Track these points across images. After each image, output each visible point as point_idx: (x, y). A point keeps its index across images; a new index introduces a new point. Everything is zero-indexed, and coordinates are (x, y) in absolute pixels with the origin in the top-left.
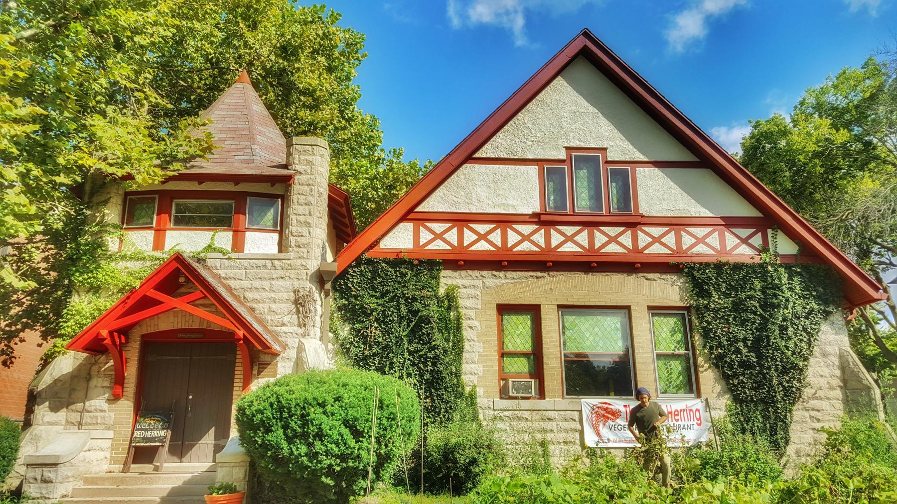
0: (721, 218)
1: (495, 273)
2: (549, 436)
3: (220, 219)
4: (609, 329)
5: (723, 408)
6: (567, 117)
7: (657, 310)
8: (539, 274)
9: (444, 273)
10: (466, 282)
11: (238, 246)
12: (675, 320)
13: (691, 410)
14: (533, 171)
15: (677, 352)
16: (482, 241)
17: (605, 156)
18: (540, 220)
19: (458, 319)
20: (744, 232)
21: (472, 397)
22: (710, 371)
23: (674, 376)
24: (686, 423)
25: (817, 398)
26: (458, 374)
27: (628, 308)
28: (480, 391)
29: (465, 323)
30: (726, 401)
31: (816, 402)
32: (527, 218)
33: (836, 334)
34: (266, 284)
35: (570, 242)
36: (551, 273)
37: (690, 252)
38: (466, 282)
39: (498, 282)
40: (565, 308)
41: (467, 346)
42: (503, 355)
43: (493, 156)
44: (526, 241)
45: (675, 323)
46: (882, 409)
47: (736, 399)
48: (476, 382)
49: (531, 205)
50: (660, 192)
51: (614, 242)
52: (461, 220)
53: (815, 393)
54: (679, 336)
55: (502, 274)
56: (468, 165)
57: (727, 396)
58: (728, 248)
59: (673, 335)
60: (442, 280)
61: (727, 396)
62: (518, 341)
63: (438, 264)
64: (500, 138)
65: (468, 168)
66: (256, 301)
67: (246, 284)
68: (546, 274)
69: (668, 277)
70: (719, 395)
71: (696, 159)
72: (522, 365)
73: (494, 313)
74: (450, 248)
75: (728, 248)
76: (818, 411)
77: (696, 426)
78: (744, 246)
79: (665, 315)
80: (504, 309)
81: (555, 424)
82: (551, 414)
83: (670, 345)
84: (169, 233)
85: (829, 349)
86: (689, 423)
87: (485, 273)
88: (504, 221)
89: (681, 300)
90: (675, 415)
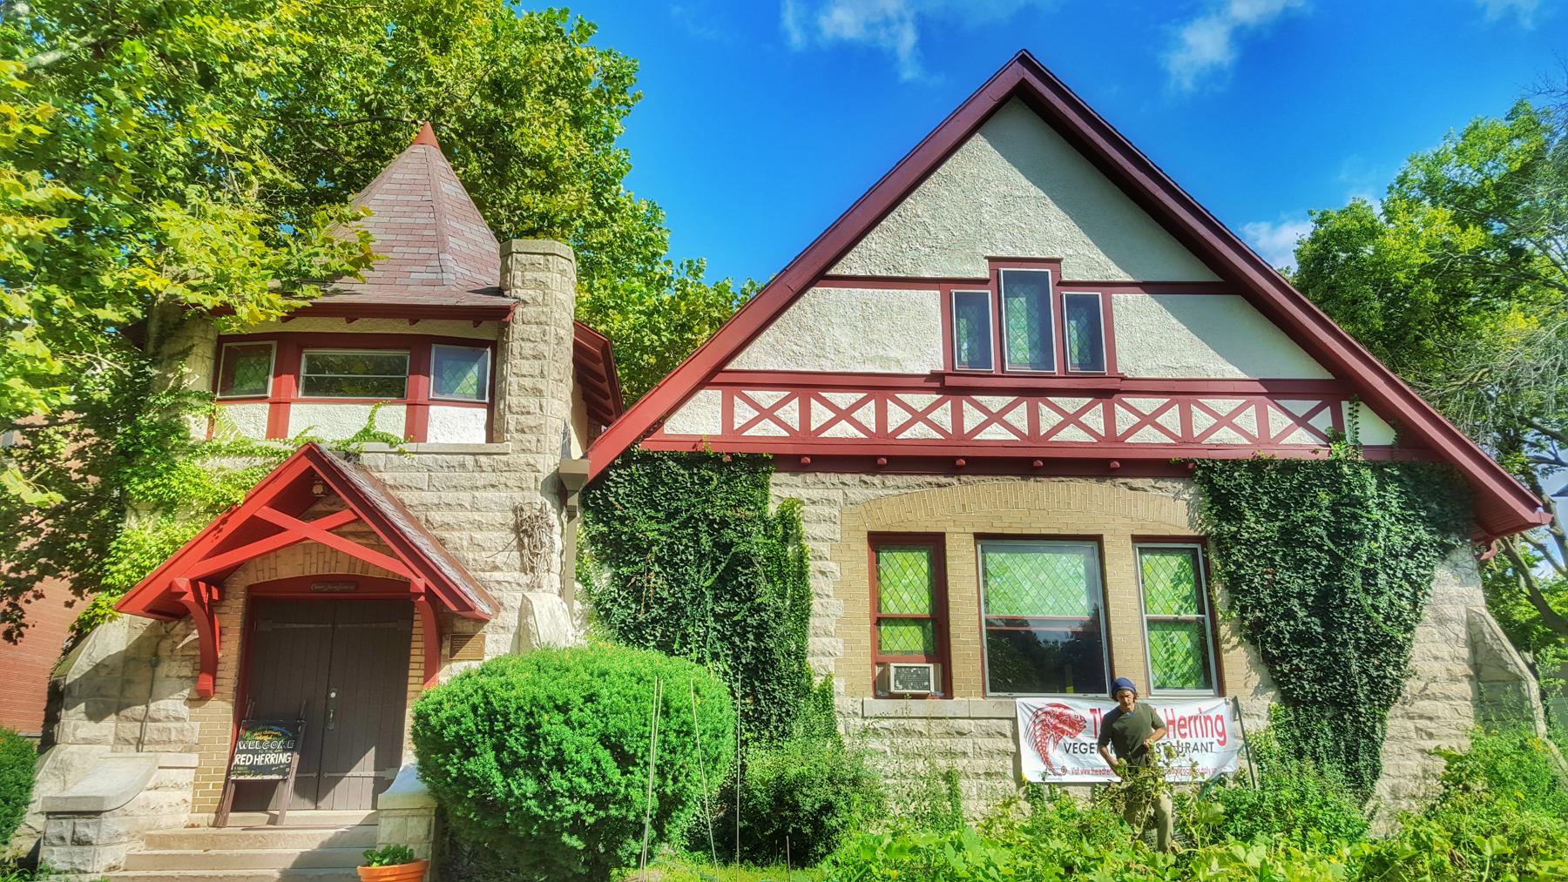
0: (1261, 381)
1: (864, 477)
4: (1064, 576)
5: (1264, 713)
6: (997, 206)
7: (1147, 543)
8: (942, 480)
9: (775, 478)
10: (815, 494)
11: (416, 430)
12: (1180, 559)
13: (1209, 718)
14: (931, 299)
15: (1183, 616)
16: (842, 422)
17: (1058, 273)
19: (801, 558)
20: (1301, 407)
21: (826, 694)
23: (1179, 658)
24: (1200, 740)
25: (1428, 697)
26: (800, 655)
27: (1098, 539)
28: (839, 685)
29: (813, 566)
30: (1268, 701)
31: (1426, 703)
32: (921, 383)
33: (1462, 584)
34: (465, 497)
35: (996, 423)
36: (963, 478)
37: (1206, 441)
38: (815, 494)
40: (987, 539)
43: (862, 273)
44: (919, 421)
45: (1180, 565)
47: (1287, 698)
48: (832, 669)
50: (1152, 337)
51: (1073, 424)
52: (806, 385)
55: (877, 480)
57: (1271, 693)
58: (1273, 435)
59: (1175, 587)
60: (773, 491)
62: (906, 597)
63: (766, 461)
64: (874, 242)
65: (818, 293)
66: (447, 526)
67: (430, 497)
71: (1217, 279)
72: (912, 639)
73: (863, 548)
74: (786, 434)
75: (1273, 435)
76: (1430, 719)
77: (1216, 745)
78: (1301, 430)
79: (1163, 551)
80: (881, 541)
81: (970, 742)
82: (964, 725)
83: (1172, 604)
84: (295, 408)
85: (1448, 610)
86: (1205, 740)
88: (881, 387)
89: (1190, 524)
90: (1180, 726)
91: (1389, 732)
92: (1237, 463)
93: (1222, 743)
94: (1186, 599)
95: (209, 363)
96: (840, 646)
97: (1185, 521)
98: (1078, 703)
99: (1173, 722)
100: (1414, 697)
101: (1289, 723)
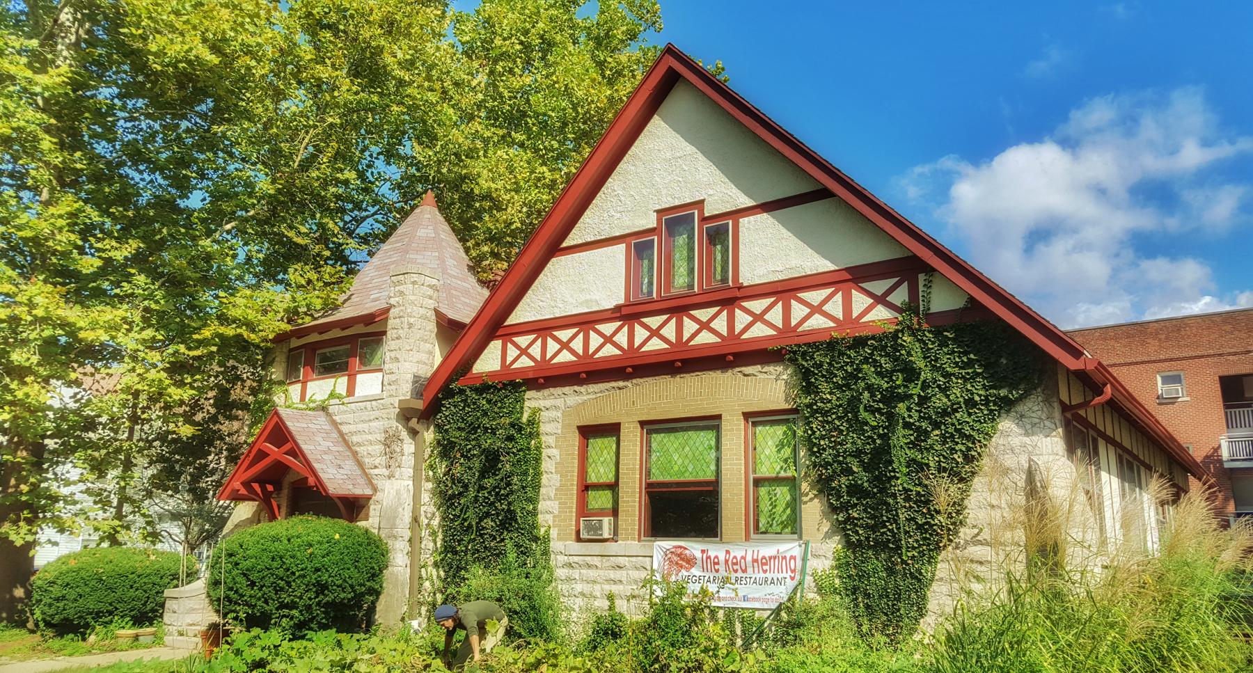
0: (846, 269)
1: (576, 388)
2: (615, 589)
3: (331, 367)
4: (701, 449)
5: (830, 555)
6: (671, 167)
7: (755, 418)
8: (621, 384)
9: (529, 394)
10: (548, 403)
11: (351, 390)
12: (784, 428)
13: (785, 558)
15: (782, 474)
16: (562, 351)
17: (701, 211)
18: (628, 314)
19: (538, 448)
20: (879, 287)
21: (547, 539)
22: (816, 500)
23: (779, 509)
24: (775, 576)
25: (980, 543)
26: (534, 513)
28: (554, 533)
29: (545, 452)
30: (834, 545)
31: (979, 548)
32: (609, 315)
33: (1027, 434)
34: (365, 426)
35: (655, 335)
36: (634, 381)
37: (800, 329)
38: (548, 403)
39: (579, 399)
40: (651, 426)
41: (544, 479)
42: (586, 488)
43: (580, 242)
44: (607, 343)
45: (785, 433)
46: (612, 576)
47: (849, 545)
48: (551, 523)
49: (612, 294)
50: (772, 249)
51: (705, 329)
52: (543, 329)
53: (978, 534)
54: (787, 452)
55: (582, 389)
56: (554, 260)
57: (837, 538)
58: (855, 315)
59: (779, 451)
60: (527, 404)
61: (837, 538)
62: (602, 470)
63: (520, 385)
64: (588, 217)
65: (558, 265)
66: (359, 444)
67: (352, 428)
68: (628, 384)
69: (771, 368)
70: (827, 536)
73: (575, 438)
75: (855, 315)
76: (981, 563)
77: (788, 580)
78: (880, 307)
79: (773, 423)
80: (588, 432)
81: (624, 572)
82: (621, 561)
83: (775, 465)
84: (359, 377)
85: (1009, 461)
86: (780, 576)
87: (567, 389)
88: (585, 322)
89: (786, 400)
90: (763, 564)
91: (939, 574)
92: (815, 346)
93: (792, 578)
94: (786, 461)
95: (284, 365)
96: (557, 507)
97: (782, 396)
98: (694, 545)
99: (755, 561)
100: (966, 541)
101: (848, 564)
